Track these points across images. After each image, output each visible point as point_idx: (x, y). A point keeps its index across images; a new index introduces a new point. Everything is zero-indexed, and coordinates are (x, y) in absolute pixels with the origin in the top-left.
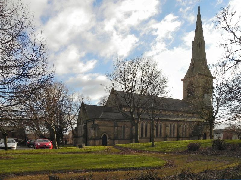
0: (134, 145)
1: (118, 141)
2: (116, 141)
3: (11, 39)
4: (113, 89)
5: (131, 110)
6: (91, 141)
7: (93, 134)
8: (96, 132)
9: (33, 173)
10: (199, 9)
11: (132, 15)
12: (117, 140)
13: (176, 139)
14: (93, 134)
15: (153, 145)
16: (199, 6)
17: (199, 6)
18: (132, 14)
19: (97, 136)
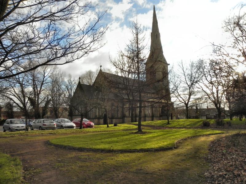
0: (99, 126)
1: (115, 119)
2: (114, 119)
3: (9, 70)
4: (79, 82)
5: (127, 92)
6: (96, 120)
7: (97, 113)
8: (100, 112)
9: (122, 141)
10: (154, 7)
11: (142, 15)
12: (114, 119)
13: (151, 118)
14: (97, 113)
15: (168, 123)
16: (154, 6)
17: (154, 6)
18: (146, 13)
19: (100, 115)
